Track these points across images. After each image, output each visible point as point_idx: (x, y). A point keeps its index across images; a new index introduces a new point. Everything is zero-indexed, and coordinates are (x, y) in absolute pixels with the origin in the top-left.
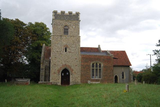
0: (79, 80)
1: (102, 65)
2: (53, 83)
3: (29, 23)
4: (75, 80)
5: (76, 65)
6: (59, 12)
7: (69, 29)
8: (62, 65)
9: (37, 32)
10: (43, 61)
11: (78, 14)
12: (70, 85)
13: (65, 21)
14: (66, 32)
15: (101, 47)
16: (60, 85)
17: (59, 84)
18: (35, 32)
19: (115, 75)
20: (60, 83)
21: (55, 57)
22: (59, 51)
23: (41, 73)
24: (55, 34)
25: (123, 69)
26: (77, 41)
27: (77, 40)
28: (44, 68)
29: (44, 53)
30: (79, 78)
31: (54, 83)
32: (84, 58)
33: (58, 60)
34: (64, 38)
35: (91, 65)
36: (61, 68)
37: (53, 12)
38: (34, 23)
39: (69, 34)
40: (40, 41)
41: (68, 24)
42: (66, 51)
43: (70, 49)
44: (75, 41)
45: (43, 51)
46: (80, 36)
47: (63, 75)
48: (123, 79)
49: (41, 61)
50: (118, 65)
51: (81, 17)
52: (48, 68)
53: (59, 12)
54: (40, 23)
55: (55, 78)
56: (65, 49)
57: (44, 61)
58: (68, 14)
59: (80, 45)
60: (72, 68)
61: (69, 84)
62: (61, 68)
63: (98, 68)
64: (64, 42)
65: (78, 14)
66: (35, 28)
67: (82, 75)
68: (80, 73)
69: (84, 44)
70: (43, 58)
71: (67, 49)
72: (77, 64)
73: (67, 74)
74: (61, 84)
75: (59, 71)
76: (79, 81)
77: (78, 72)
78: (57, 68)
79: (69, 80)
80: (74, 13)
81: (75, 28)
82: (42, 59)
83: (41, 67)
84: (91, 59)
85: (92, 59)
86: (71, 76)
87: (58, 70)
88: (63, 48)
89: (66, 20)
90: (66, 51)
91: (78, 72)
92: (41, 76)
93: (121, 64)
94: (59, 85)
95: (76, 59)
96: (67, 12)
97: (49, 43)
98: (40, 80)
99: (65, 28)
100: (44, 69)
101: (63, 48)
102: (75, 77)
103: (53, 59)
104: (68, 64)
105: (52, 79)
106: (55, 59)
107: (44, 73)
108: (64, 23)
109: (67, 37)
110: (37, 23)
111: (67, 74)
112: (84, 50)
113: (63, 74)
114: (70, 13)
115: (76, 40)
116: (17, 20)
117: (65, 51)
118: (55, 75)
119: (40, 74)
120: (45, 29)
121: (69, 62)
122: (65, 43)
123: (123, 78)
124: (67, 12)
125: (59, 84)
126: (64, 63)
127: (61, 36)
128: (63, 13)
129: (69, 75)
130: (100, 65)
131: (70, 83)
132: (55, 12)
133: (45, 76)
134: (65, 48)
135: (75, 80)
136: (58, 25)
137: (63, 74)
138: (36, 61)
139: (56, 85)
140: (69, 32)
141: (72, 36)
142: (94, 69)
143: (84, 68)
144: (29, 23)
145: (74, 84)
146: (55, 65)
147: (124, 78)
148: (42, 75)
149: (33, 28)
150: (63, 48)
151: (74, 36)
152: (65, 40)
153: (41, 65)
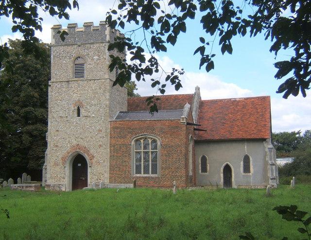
1: (159, 143)
4: (97, 180)
7: (85, 65)
15: (201, 91)
19: (224, 165)
25: (246, 149)
26: (101, 91)
30: (107, 175)
32: (117, 128)
39: (85, 75)
41: (83, 52)
42: (79, 115)
48: (248, 174)
50: (232, 138)
58: (99, 28)
60: (92, 151)
63: (142, 150)
68: (107, 164)
71: (82, 111)
75: (63, 159)
81: (98, 59)
85: (136, 129)
87: (62, 158)
88: (73, 108)
90: (79, 115)
93: (242, 135)
95: (100, 131)
99: (76, 63)
101: (73, 108)
105: (51, 178)
109: (81, 83)
116: (202, 21)
117: (76, 115)
118: (58, 169)
123: (247, 169)
126: (75, 142)
127: (68, 82)
130: (154, 141)
134: (76, 108)
136: (62, 57)
141: (90, 80)
142: (144, 149)
146: (57, 146)
147: (250, 172)
150: (73, 108)
151: (95, 80)
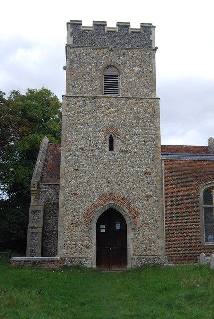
0: (159, 249)
2: (67, 262)
3: (12, 93)
4: (145, 250)
5: (148, 196)
6: (87, 23)
7: (120, 77)
8: (100, 197)
9: (29, 113)
10: (39, 185)
11: (147, 29)
12: (129, 266)
13: (105, 51)
14: (111, 85)
16: (94, 266)
17: (91, 263)
18: (24, 111)
20: (94, 260)
21: (76, 168)
22: (87, 147)
23: (30, 225)
24: (74, 93)
26: (148, 115)
27: (150, 110)
28: (42, 208)
29: (42, 163)
30: (161, 243)
31: (71, 259)
32: (175, 170)
33: (82, 182)
34: (104, 103)
35: (201, 194)
36: (95, 207)
37: (69, 26)
38: (24, 93)
39: (120, 92)
40: (36, 135)
41: (116, 59)
42: (111, 149)
43: (125, 141)
44: (144, 115)
45: (40, 156)
46: (157, 97)
47: (103, 231)
49: (32, 186)
51: (159, 39)
52: (51, 210)
53: (87, 23)
54: (40, 93)
55: (77, 243)
56: (108, 142)
57: (42, 186)
58: (117, 30)
59: (158, 138)
60: (135, 205)
61: (127, 265)
62: (95, 207)
64: (106, 118)
65: (147, 29)
66: (27, 102)
67: (170, 233)
68: (161, 225)
69: (166, 140)
70: (39, 176)
71: (118, 143)
72: (149, 193)
73: (118, 227)
74: (99, 261)
76: (162, 253)
77: (156, 221)
78: (82, 208)
79: (126, 250)
80: (135, 25)
81: (140, 71)
82: (34, 181)
83: (33, 204)
84: (200, 173)
86: (131, 235)
89: (111, 47)
90: (111, 149)
91: (156, 221)
92: (29, 236)
94: (91, 269)
95: (147, 173)
96: (112, 24)
97: (56, 135)
98: (29, 249)
100: (42, 213)
101: (103, 138)
102: (146, 240)
103: (68, 176)
104: (117, 191)
106: (74, 175)
107: (41, 225)
108: (103, 57)
109: (115, 101)
110: (31, 92)
111: (118, 227)
112: (167, 149)
113: (103, 226)
114: (124, 26)
115: (146, 111)
117: (108, 148)
118: (77, 231)
119: (29, 230)
120: (52, 103)
121: (124, 185)
122: (107, 121)
124: (112, 24)
125: (89, 266)
126: (106, 190)
127: (94, 98)
128: (99, 26)
129: (124, 233)
131: (129, 261)
132: (74, 26)
133: (44, 235)
134: (108, 137)
135: (145, 250)
137: (103, 226)
138: (26, 191)
139: (78, 267)
140: (120, 86)
141: (130, 98)
143: (177, 207)
144: (12, 93)
145: (144, 267)
146: (75, 195)
148: (34, 230)
149: (20, 103)
150: (103, 138)
152: (108, 114)
153: (33, 198)
